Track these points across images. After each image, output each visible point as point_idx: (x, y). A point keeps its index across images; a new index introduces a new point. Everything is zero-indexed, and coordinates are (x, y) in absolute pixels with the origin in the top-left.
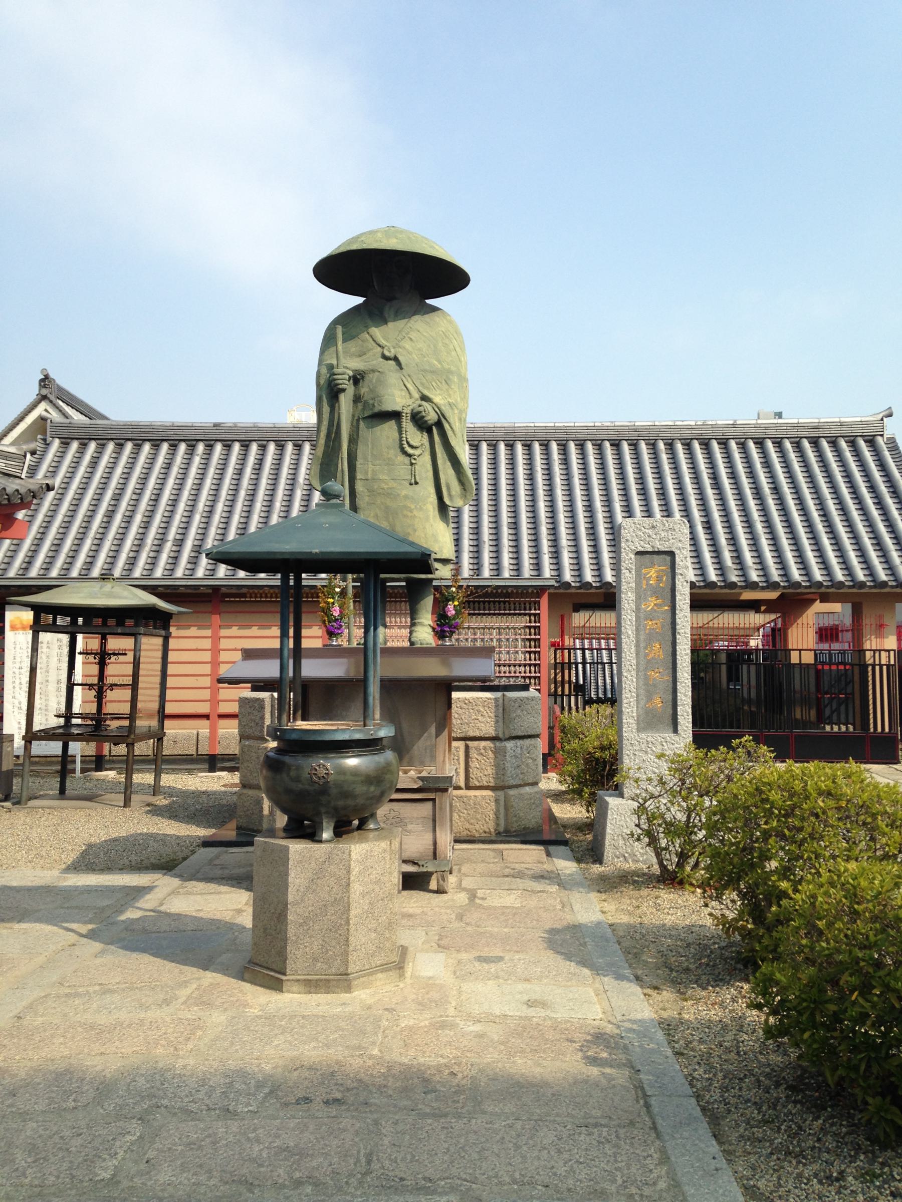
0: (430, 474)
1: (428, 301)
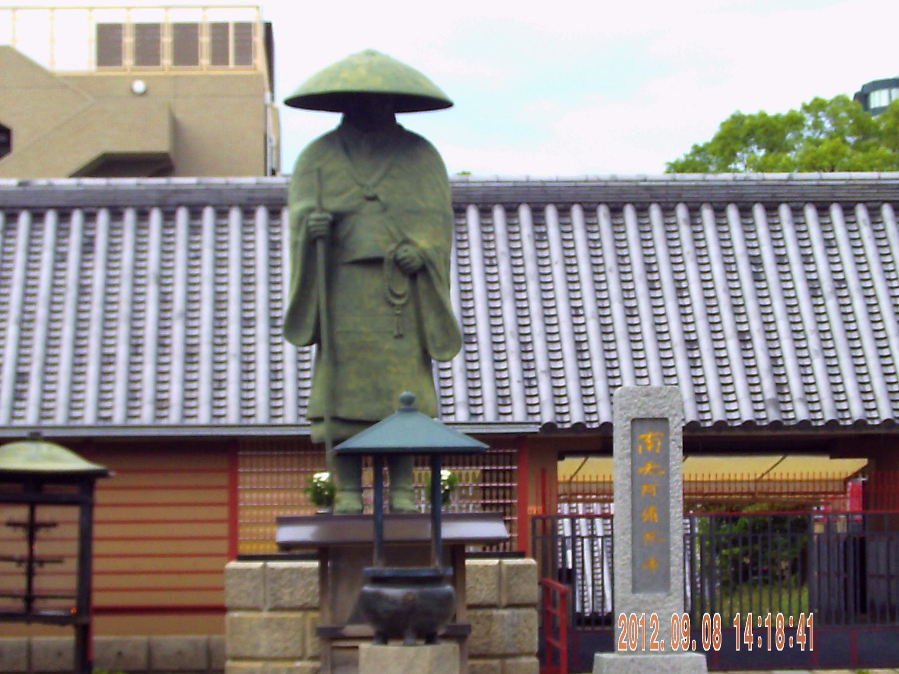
0: (414, 325)
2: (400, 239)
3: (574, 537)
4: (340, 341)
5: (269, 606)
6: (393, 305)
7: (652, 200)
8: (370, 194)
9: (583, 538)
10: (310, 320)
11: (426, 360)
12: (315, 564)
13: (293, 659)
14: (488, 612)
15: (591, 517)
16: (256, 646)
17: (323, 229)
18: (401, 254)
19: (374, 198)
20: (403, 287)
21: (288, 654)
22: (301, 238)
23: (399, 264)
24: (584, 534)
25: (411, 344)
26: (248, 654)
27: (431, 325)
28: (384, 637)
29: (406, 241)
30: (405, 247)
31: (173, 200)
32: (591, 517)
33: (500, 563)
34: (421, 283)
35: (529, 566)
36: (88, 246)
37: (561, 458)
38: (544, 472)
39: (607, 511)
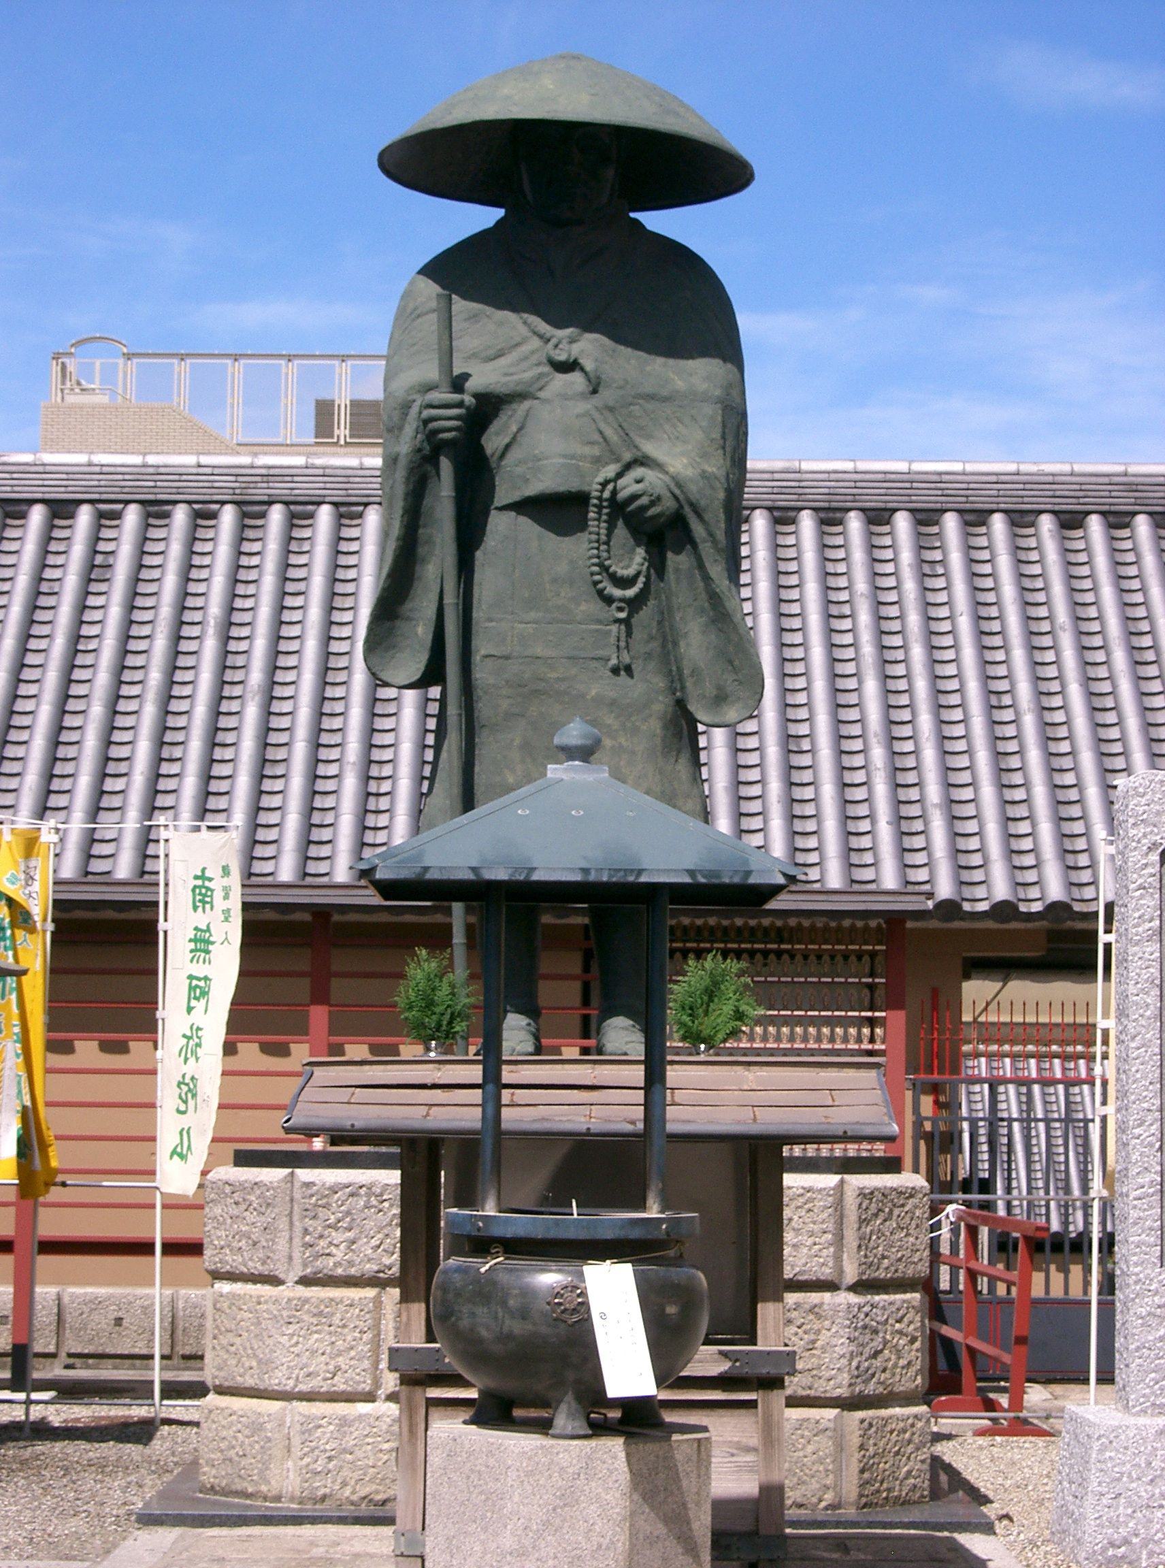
1: (656, 221)
2: (627, 456)
3: (994, 1120)
4: (482, 674)
5: (298, 1272)
6: (609, 600)
7: (1137, 508)
8: (562, 357)
9: (1010, 1120)
10: (423, 631)
11: (683, 733)
12: (393, 1177)
13: (350, 1398)
14: (814, 1297)
15: (1023, 1082)
16: (267, 1365)
17: (449, 423)
18: (627, 486)
19: (569, 366)
20: (634, 562)
21: (340, 1385)
22: (995, 1241)
23: (620, 510)
24: (1040, 1115)
25: (647, 686)
26: (250, 1382)
27: (696, 644)
28: (495, 1412)
29: (642, 461)
30: (639, 472)
31: (260, 493)
32: (1023, 1082)
33: (842, 1182)
34: (677, 561)
35: (912, 1193)
36: (95, 570)
37: (967, 976)
38: (935, 993)
39: (1072, 1074)
